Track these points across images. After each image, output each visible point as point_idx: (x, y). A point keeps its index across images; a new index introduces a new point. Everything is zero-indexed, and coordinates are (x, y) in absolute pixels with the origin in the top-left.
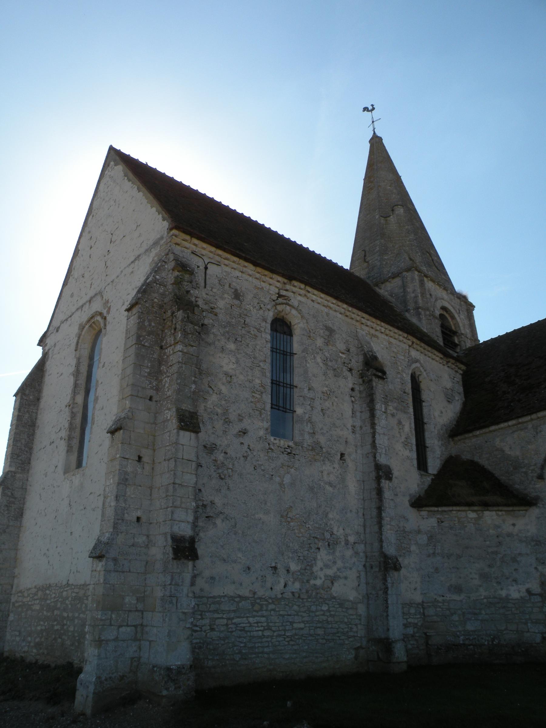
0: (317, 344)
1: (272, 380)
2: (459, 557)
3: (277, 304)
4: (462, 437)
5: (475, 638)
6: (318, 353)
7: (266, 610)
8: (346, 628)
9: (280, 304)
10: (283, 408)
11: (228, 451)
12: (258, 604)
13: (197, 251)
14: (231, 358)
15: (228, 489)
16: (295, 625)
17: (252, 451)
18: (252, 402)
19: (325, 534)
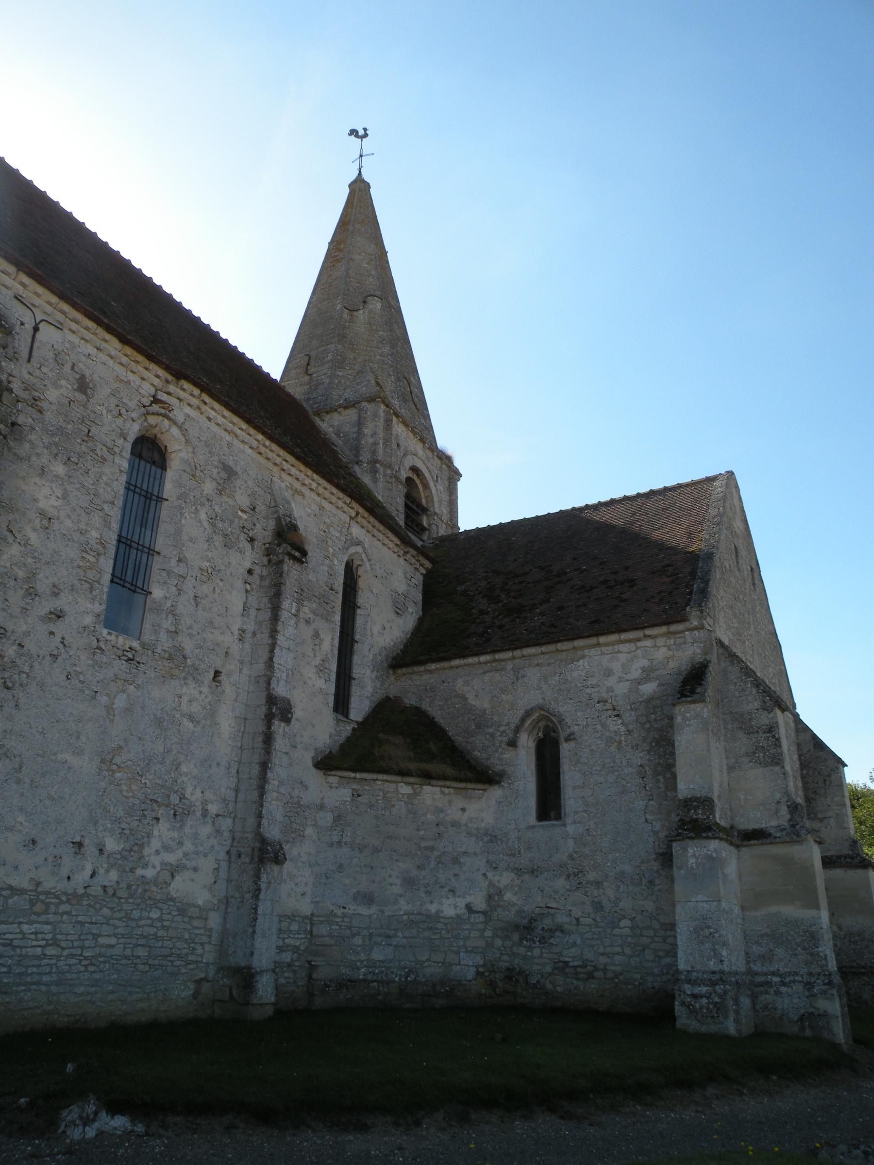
0: (203, 490)
1: (120, 536)
2: (376, 850)
3: (148, 413)
4: (409, 670)
5: (382, 972)
6: (204, 505)
7: (55, 913)
8: (185, 948)
9: (153, 414)
10: (132, 584)
11: (26, 642)
12: (43, 902)
13: (24, 296)
14: (54, 489)
15: (17, 706)
16: (101, 940)
17: (68, 649)
18: (79, 567)
19: (172, 798)
